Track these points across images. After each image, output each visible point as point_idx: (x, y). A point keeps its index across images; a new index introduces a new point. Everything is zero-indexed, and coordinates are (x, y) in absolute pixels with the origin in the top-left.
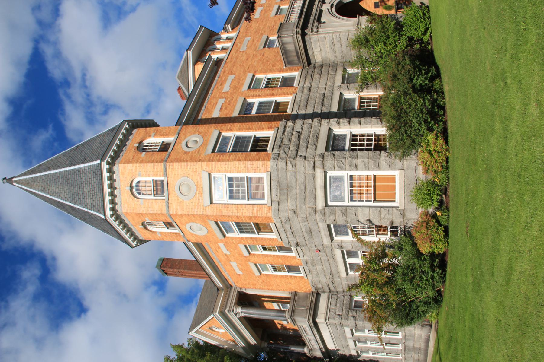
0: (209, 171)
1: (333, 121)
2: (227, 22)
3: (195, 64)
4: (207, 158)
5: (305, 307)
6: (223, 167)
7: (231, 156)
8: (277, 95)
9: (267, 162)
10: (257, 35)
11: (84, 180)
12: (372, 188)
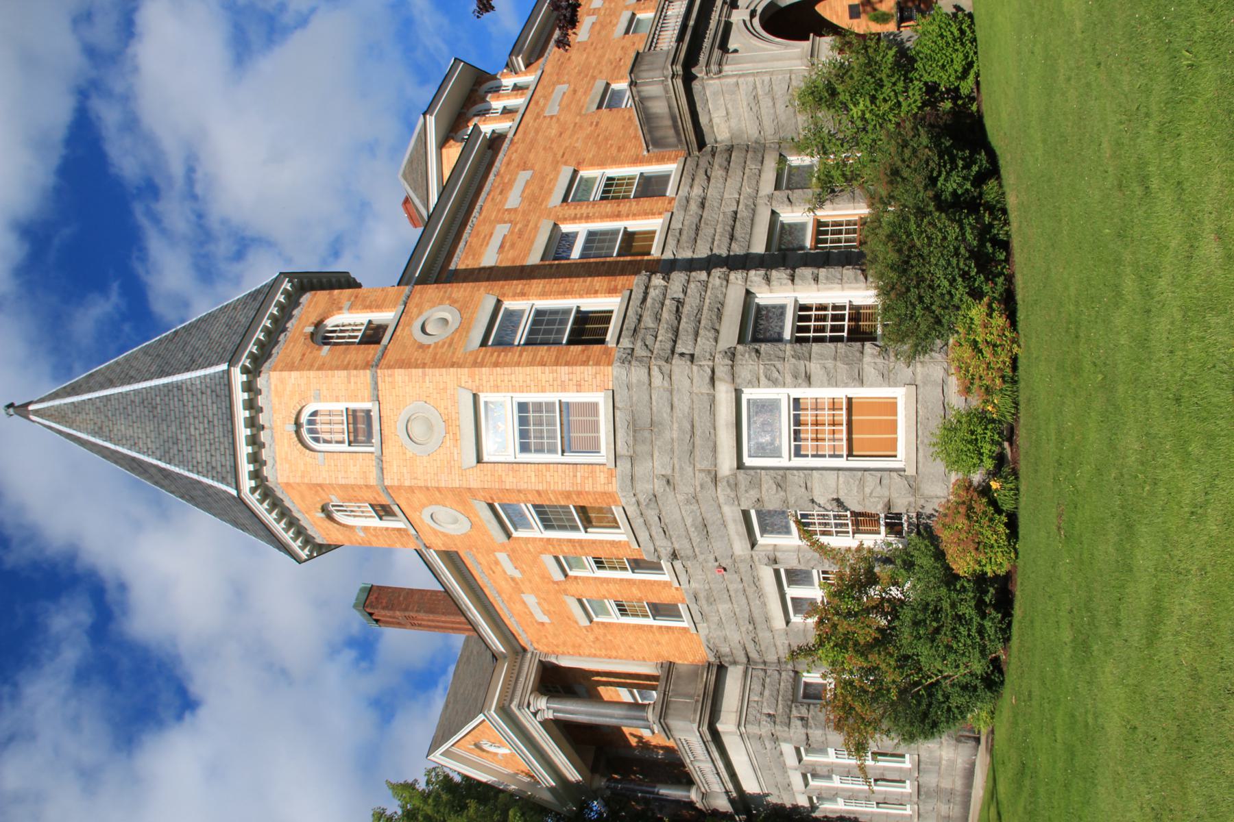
1: (755, 275)
2: (515, 51)
3: (442, 144)
4: (470, 359)
5: (691, 697)
6: (506, 380)
7: (525, 354)
8: (628, 216)
9: (606, 368)
10: (582, 80)
11: (191, 410)
12: (844, 428)
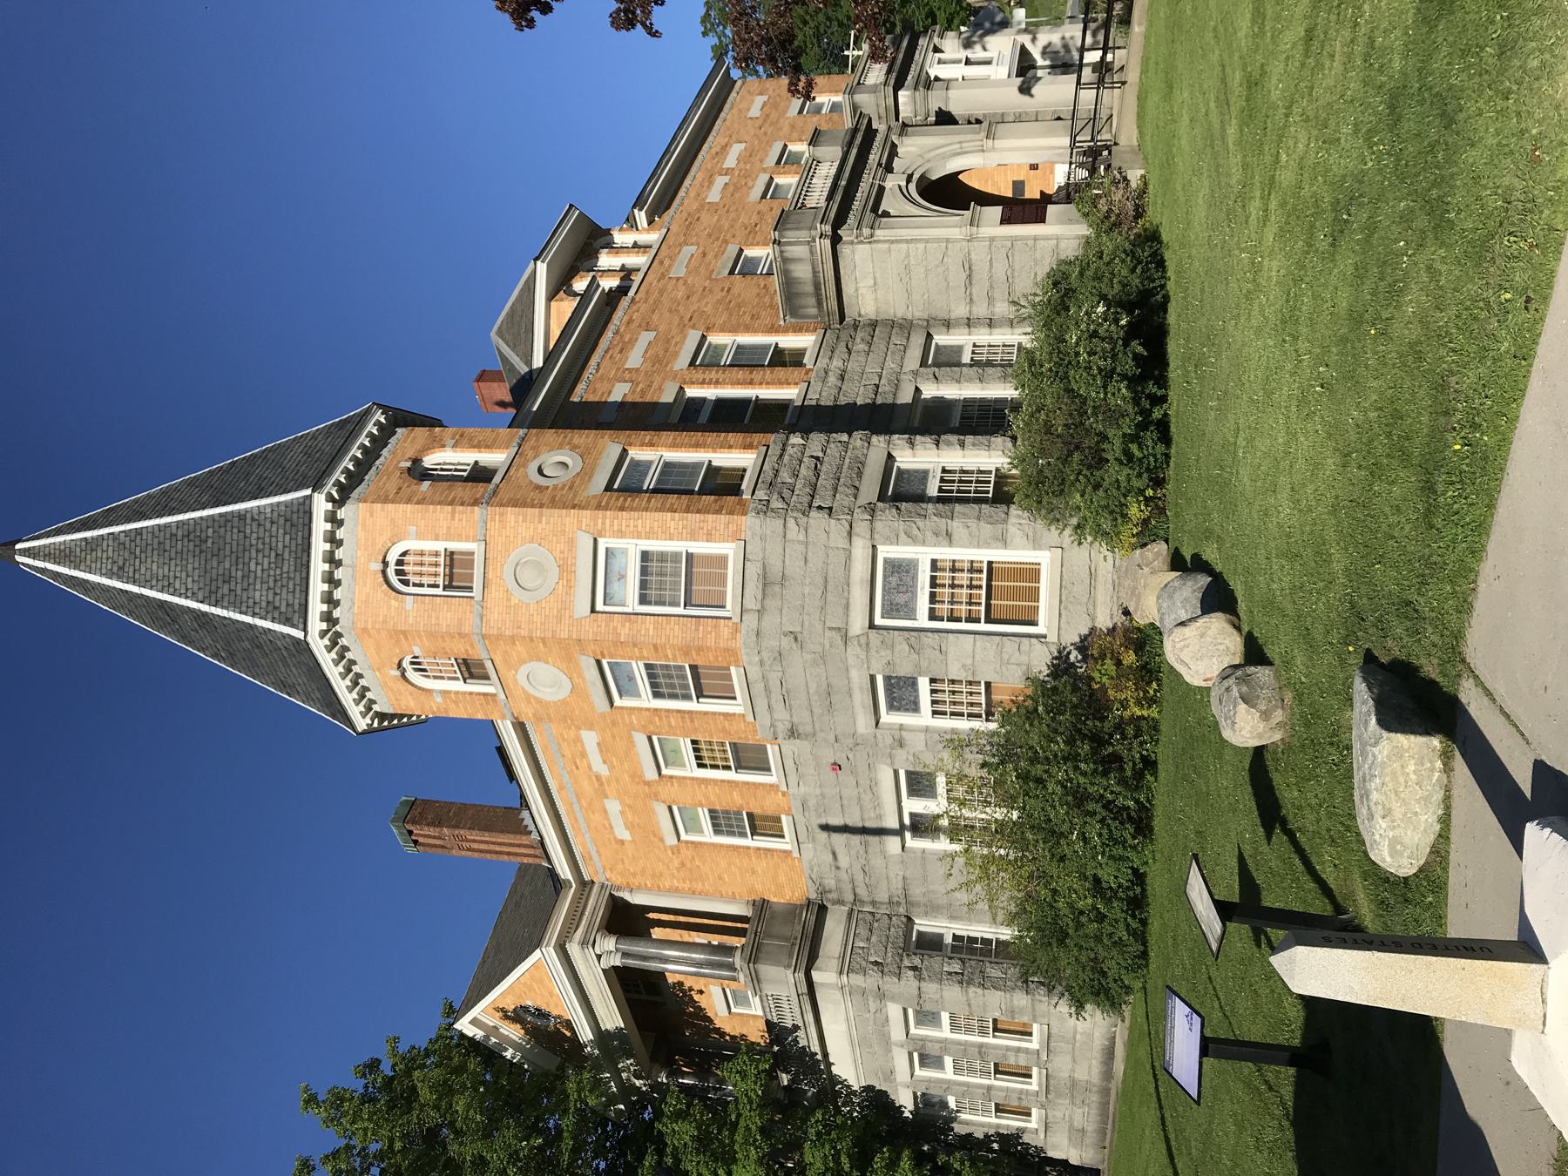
0: (596, 532)
1: (899, 439)
2: (639, 203)
3: (551, 296)
4: (594, 503)
5: (786, 939)
6: (632, 525)
7: (653, 500)
8: (761, 384)
9: (740, 517)
10: (713, 243)
11: (254, 542)
12: (983, 592)
